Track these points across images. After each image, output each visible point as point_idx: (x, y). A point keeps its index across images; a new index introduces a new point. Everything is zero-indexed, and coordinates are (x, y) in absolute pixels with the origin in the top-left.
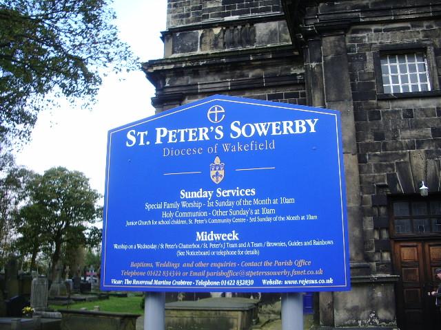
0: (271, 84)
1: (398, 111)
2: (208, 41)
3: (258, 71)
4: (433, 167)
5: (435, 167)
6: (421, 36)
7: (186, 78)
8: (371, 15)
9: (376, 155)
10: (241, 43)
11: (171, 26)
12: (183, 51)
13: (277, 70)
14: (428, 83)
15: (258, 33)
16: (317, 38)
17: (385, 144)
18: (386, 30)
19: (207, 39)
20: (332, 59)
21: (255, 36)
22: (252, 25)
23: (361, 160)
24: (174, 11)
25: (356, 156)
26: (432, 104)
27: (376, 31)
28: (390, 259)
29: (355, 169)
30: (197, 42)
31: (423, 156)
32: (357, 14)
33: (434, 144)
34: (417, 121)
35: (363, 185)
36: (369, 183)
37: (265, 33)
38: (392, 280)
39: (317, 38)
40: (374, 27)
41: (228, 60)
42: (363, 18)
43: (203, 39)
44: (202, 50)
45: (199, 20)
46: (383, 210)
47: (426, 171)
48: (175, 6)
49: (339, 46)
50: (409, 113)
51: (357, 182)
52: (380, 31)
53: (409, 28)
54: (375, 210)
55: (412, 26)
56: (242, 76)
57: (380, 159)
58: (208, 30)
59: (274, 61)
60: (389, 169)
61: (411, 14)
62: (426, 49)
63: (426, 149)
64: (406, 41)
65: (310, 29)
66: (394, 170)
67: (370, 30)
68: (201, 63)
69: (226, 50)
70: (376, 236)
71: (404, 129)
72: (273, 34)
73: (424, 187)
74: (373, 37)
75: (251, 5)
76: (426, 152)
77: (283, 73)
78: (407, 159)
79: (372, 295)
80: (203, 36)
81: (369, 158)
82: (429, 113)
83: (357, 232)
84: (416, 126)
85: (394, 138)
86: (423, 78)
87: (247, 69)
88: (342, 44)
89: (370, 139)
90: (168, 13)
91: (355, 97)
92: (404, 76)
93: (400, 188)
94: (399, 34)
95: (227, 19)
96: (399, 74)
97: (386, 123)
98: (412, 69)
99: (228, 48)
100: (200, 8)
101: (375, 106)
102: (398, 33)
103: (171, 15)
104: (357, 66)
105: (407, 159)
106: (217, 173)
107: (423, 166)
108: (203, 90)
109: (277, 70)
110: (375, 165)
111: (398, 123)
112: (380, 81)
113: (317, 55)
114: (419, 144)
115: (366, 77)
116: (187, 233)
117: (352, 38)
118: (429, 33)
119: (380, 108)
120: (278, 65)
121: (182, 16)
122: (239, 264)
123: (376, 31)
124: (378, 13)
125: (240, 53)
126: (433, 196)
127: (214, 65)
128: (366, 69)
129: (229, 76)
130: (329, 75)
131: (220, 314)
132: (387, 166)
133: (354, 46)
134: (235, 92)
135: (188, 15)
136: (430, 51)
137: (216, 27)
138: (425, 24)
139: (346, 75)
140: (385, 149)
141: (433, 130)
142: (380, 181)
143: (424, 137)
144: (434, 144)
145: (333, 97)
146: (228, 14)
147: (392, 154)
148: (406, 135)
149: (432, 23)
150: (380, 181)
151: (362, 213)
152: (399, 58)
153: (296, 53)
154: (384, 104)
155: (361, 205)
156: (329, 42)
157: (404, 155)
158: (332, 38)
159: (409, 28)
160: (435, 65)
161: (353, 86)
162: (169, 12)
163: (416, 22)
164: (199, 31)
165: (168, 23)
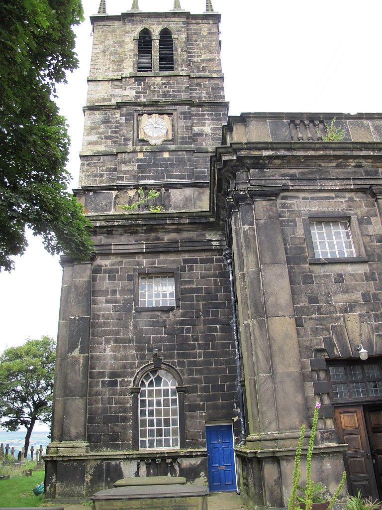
0: (186, 249)
1: (329, 276)
3: (173, 236)
4: (367, 330)
5: (369, 331)
6: (344, 206)
7: (99, 237)
8: (299, 183)
9: (311, 319)
11: (84, 185)
12: (96, 210)
13: (193, 235)
14: (353, 250)
15: (173, 198)
16: (249, 202)
17: (319, 308)
18: (312, 199)
19: (121, 200)
20: (265, 223)
21: (170, 201)
22: (167, 190)
23: (299, 324)
24: (87, 171)
25: (294, 319)
27: (304, 199)
29: (293, 333)
30: (111, 203)
31: (357, 319)
32: (286, 182)
33: (365, 308)
34: (347, 286)
35: (303, 350)
36: (307, 347)
37: (180, 198)
38: (341, 449)
39: (249, 202)
40: (301, 195)
41: (144, 223)
42: (292, 186)
43: (118, 200)
44: (115, 210)
45: (113, 181)
46: (322, 375)
47: (361, 335)
48: (88, 165)
49: (271, 210)
50: (340, 279)
51: (296, 346)
52: (308, 199)
53: (333, 198)
54: (315, 375)
55: (336, 197)
57: (316, 323)
58: (123, 191)
59: (190, 226)
60: (326, 332)
61: (335, 185)
62: (350, 217)
63: (359, 312)
64: (331, 210)
65: (242, 193)
66: (330, 334)
67: (298, 197)
68: (116, 224)
69: (141, 212)
70: (318, 404)
71: (336, 293)
72: (188, 201)
73: (363, 350)
74: (302, 204)
75: (167, 171)
76: (361, 316)
77: (198, 239)
78: (341, 323)
79: (321, 468)
80: (117, 196)
81: (305, 322)
82: (358, 278)
83: (299, 399)
84: (347, 290)
85: (328, 302)
86: (349, 246)
87: (163, 232)
88: (274, 209)
89: (304, 303)
90: (224, 96)
91: (288, 261)
92: (331, 242)
93: (337, 353)
94: (325, 202)
95: (142, 182)
97: (319, 287)
98: (330, 237)
99: (143, 211)
100: (115, 169)
101: (307, 270)
103: (84, 174)
104: (288, 231)
105: (341, 323)
107: (358, 330)
108: (117, 251)
109: (193, 235)
110: (311, 328)
111: (330, 287)
112: (311, 246)
113: (249, 219)
114: (350, 308)
115: (297, 241)
117: (282, 204)
118: (351, 204)
119: (311, 272)
120: (193, 231)
121: (96, 176)
123: (304, 199)
124: (305, 182)
125: (157, 216)
126: (374, 360)
128: (296, 234)
129: (144, 238)
130: (263, 238)
131: (175, 501)
132: (323, 329)
133: (284, 212)
134: (150, 255)
135: (102, 176)
136: (354, 220)
137: (131, 189)
138: (347, 195)
139: (280, 238)
140: (320, 313)
141: (363, 295)
142: (317, 345)
143: (356, 301)
144: (365, 308)
145: (267, 259)
146: (143, 178)
147: (327, 317)
150: (317, 345)
151: (304, 378)
152: (325, 226)
153: (212, 220)
154: (315, 268)
155: (302, 369)
156: (261, 206)
157: (338, 319)
158: (265, 203)
159: (333, 198)
160: (360, 233)
161: (286, 249)
162: (82, 171)
164: (113, 192)
165: (80, 181)
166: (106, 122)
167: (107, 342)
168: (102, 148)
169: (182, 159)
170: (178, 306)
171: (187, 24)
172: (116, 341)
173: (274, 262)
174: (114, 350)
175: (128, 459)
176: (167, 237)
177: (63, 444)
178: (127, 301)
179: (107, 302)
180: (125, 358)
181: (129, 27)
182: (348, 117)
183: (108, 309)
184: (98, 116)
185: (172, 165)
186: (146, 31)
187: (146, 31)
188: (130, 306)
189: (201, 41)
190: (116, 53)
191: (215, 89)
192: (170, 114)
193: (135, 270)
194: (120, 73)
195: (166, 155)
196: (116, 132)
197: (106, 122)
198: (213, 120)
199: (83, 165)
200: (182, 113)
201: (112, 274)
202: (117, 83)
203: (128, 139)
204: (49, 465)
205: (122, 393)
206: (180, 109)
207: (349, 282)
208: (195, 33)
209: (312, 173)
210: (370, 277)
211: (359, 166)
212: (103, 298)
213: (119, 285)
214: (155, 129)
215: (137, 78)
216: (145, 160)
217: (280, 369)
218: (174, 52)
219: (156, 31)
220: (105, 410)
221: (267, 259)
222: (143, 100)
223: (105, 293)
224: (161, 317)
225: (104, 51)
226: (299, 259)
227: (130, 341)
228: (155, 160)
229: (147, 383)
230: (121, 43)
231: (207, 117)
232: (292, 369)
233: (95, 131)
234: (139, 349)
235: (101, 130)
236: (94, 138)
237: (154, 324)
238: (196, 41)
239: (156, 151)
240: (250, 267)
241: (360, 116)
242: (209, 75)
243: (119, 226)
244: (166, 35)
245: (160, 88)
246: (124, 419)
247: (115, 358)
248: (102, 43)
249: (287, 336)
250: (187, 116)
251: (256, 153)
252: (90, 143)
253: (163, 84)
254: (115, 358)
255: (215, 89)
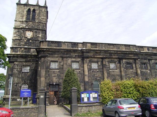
2: (21, 51)
3: (30, 58)
6: (57, 60)
7: (15, 58)
10: (27, 52)
12: (15, 52)
22: (30, 49)
23: (46, 79)
26: (58, 70)
28: (150, 69)
29: (44, 80)
56: (27, 59)
73: (54, 83)
84: (55, 74)
86: (57, 66)
92: (54, 66)
93: (51, 83)
95: (25, 47)
96: (55, 65)
100: (20, 43)
102: (54, 58)
106: (26, 92)
116: (24, 95)
122: (26, 96)
127: (22, 56)
135: (17, 44)
148: (53, 75)
149: (60, 57)
154: (50, 70)
156: (42, 59)
162: (12, 43)
163: (57, 57)
165: (12, 45)
166: (18, 32)
167: (16, 78)
168: (17, 38)
169: (34, 42)
170: (30, 72)
171: (39, 8)
172: (18, 78)
173: (43, 69)
174: (17, 79)
175: (18, 98)
176: (29, 59)
177: (7, 95)
178: (20, 70)
179: (16, 70)
180: (19, 81)
181: (26, 7)
182: (62, 42)
183: (16, 72)
184: (17, 30)
185: (32, 43)
186: (29, 9)
187: (29, 9)
188: (20, 72)
189: (42, 13)
190: (22, 14)
191: (43, 26)
192: (33, 31)
193: (22, 65)
194: (23, 20)
195: (31, 41)
196: (20, 34)
197: (18, 32)
198: (42, 33)
199: (13, 41)
200: (35, 32)
201: (18, 65)
202: (21, 22)
203: (23, 37)
204: (8, 93)
205: (18, 87)
206: (35, 30)
207: (55, 72)
208: (41, 11)
209: (53, 53)
210: (59, 72)
211: (62, 52)
212: (16, 70)
213: (19, 67)
214: (29, 35)
215: (26, 22)
216: (26, 42)
217: (41, 85)
218: (36, 11)
219: (32, 9)
220: (15, 90)
221: (42, 68)
222: (27, 28)
223: (16, 69)
224: (27, 74)
225: (19, 13)
226: (48, 68)
227: (20, 78)
228: (28, 42)
229: (23, 85)
230: (23, 11)
231: (40, 33)
232: (43, 86)
233: (16, 34)
234: (22, 79)
235: (17, 34)
236: (15, 35)
237: (25, 75)
238: (41, 13)
239: (29, 40)
240: (39, 69)
241: (65, 42)
242: (42, 22)
243: (19, 56)
244: (34, 10)
245: (31, 25)
246: (18, 91)
247: (17, 81)
248: (19, 11)
249: (43, 81)
250: (36, 32)
251: (43, 50)
252: (14, 37)
253: (32, 24)
254: (17, 81)
255: (43, 26)
